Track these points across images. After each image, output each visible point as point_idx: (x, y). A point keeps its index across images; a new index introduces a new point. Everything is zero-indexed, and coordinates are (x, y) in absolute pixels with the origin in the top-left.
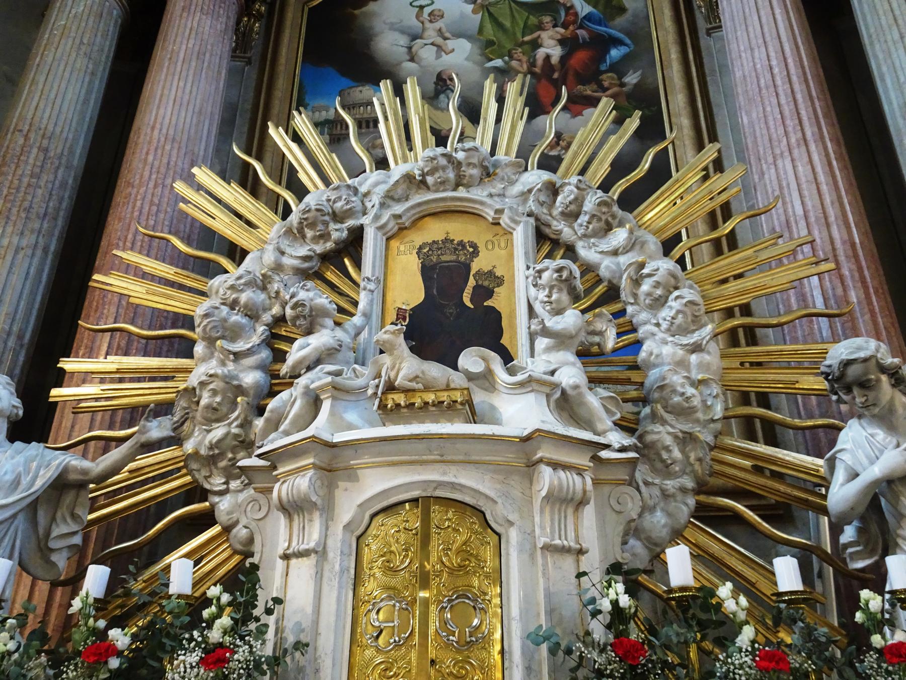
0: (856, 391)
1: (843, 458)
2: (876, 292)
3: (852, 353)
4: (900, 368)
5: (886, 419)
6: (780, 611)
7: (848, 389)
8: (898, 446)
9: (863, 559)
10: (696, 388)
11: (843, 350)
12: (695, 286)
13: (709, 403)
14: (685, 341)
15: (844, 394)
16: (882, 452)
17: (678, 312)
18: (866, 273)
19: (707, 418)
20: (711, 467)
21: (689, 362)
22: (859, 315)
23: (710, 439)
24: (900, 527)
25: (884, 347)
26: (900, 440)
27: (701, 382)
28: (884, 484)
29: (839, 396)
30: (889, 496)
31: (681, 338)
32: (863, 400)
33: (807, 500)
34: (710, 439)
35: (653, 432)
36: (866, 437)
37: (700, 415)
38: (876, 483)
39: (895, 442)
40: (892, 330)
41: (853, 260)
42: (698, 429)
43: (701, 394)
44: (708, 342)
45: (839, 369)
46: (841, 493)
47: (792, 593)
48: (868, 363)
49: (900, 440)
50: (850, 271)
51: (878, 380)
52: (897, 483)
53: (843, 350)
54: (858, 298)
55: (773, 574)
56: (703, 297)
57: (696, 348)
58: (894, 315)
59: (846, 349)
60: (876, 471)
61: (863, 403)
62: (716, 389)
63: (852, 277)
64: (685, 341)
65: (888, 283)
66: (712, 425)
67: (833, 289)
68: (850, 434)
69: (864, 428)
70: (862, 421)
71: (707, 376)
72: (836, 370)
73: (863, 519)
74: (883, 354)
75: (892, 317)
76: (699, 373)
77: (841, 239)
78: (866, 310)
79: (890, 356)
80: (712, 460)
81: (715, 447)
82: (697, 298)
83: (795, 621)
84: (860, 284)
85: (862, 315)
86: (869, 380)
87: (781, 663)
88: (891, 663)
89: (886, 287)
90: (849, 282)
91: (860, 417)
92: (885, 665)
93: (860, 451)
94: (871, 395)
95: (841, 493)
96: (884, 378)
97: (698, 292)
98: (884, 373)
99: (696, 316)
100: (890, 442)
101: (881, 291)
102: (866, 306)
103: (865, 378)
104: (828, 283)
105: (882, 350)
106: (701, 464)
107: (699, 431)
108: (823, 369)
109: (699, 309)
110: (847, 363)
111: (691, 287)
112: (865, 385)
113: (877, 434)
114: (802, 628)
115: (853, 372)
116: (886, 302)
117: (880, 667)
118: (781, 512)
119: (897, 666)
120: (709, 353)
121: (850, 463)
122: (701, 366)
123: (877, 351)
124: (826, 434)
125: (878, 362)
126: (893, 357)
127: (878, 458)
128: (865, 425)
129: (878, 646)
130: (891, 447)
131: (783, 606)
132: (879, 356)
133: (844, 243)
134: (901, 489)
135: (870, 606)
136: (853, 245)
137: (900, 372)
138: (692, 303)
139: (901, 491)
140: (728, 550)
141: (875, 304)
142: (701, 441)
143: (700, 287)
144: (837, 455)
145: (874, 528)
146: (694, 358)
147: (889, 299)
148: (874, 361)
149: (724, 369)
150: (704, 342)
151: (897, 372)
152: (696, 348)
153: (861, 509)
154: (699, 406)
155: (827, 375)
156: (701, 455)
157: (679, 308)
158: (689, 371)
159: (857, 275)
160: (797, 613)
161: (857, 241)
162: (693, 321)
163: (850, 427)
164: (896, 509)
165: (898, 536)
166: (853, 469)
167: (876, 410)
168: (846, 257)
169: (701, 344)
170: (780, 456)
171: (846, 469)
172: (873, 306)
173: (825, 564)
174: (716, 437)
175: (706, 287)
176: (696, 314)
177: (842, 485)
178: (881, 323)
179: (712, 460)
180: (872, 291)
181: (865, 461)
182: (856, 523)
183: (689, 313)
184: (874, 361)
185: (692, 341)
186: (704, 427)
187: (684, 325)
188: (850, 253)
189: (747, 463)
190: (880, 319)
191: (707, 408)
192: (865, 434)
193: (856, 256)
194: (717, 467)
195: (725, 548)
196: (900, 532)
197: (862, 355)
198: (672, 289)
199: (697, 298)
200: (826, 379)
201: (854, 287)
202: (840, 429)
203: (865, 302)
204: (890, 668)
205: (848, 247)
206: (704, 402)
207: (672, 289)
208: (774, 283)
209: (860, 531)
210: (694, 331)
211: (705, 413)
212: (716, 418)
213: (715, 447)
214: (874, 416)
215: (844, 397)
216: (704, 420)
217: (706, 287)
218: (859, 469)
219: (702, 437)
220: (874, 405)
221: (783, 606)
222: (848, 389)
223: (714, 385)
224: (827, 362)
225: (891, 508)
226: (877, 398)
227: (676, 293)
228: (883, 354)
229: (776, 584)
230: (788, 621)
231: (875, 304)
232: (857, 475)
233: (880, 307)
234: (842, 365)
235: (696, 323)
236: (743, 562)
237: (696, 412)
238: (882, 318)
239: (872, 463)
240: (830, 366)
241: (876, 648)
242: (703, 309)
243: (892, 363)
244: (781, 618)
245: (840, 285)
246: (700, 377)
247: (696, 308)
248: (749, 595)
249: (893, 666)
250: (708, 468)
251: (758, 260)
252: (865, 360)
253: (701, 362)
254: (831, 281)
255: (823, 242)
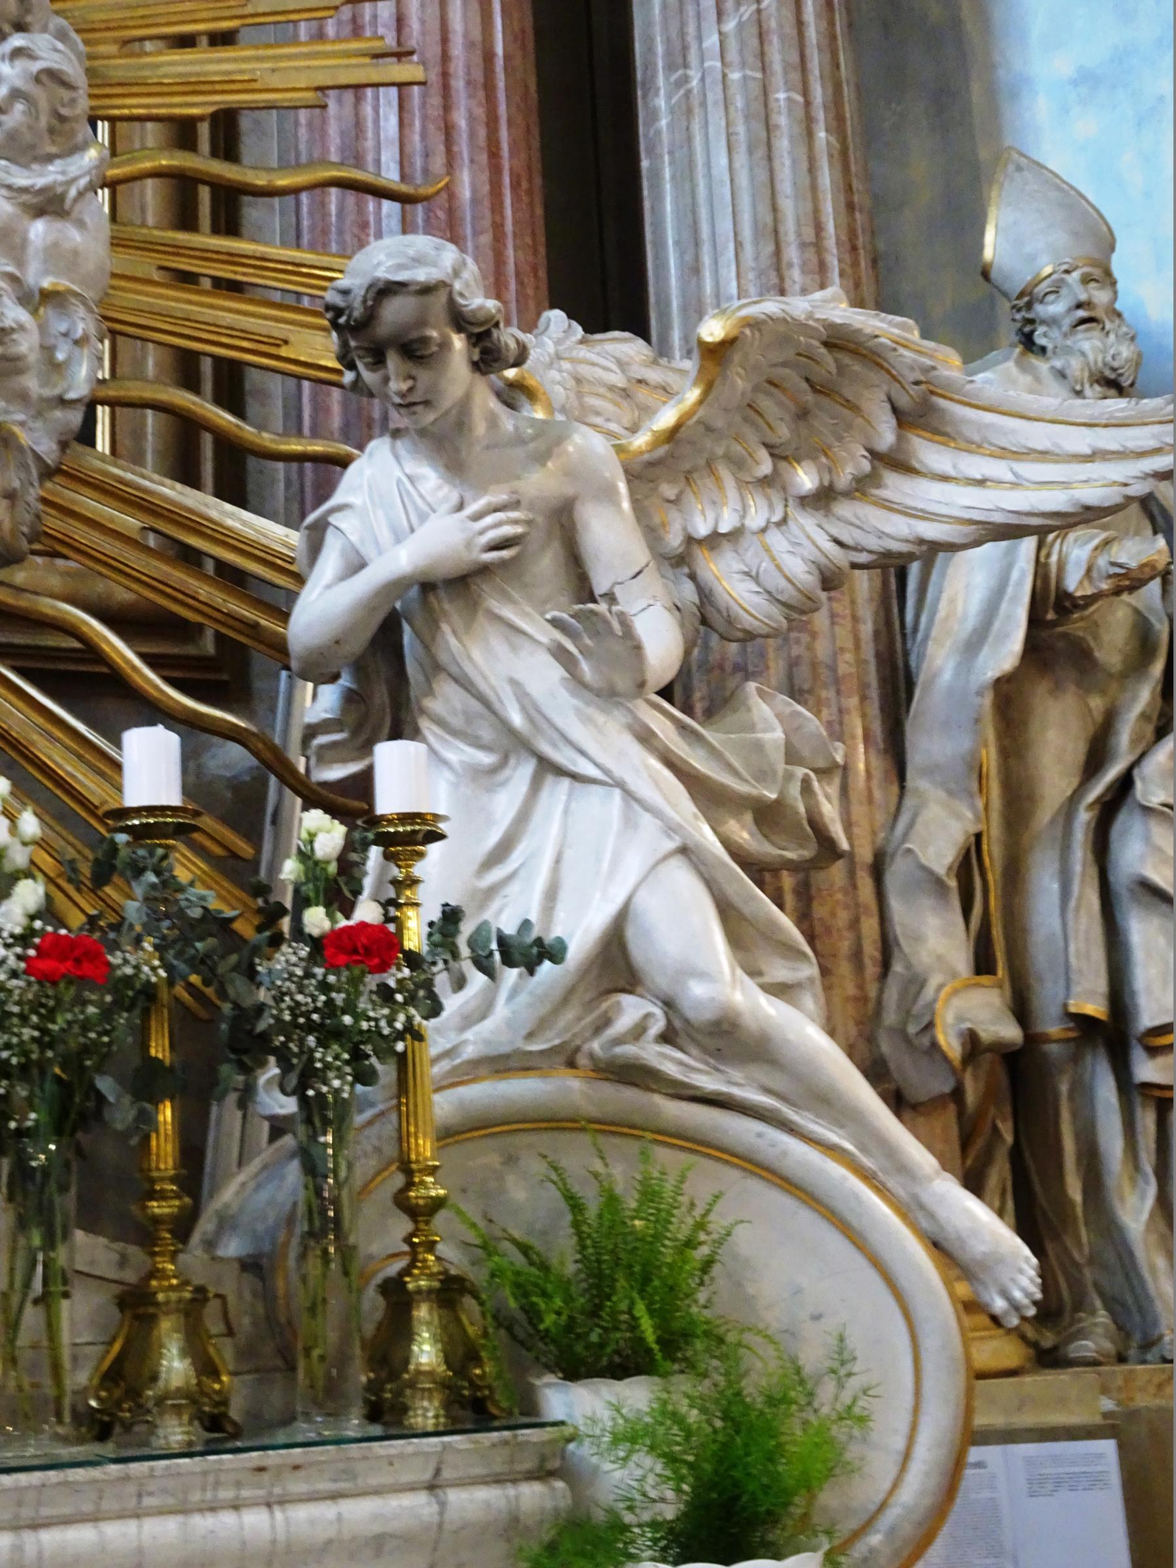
0: (393, 361)
1: (342, 526)
2: (515, 186)
3: (401, 267)
4: (497, 325)
5: (447, 444)
6: (114, 848)
7: (378, 359)
8: (460, 507)
9: (344, 761)
10: (34, 312)
11: (382, 257)
12: (74, 35)
13: (60, 356)
14: (22, 178)
15: (366, 365)
16: (423, 518)
17: (16, 94)
18: (504, 134)
19: (48, 392)
20: (38, 517)
21: (25, 242)
22: (469, 231)
23: (47, 448)
24: (430, 692)
25: (471, 269)
26: (468, 495)
27: (48, 296)
28: (414, 592)
29: (358, 375)
30: (419, 621)
31: (14, 168)
32: (404, 386)
33: (255, 626)
34: (47, 448)
35: (1028, 1295)
36: (399, 482)
37: (32, 383)
38: (397, 586)
39: (454, 498)
40: (529, 281)
41: (481, 94)
42: (21, 417)
43: (43, 328)
44: (81, 194)
45: (364, 301)
46: (323, 606)
47: (151, 810)
48: (429, 299)
49: (468, 495)
50: (471, 119)
51: (445, 345)
52: (442, 593)
53: (382, 257)
54: (474, 190)
55: (118, 767)
56: (90, 72)
57: (49, 204)
58: (542, 250)
59: (389, 255)
60: (399, 559)
61: (403, 395)
62: (83, 323)
63: (472, 135)
64: (22, 178)
65: (545, 176)
66: (58, 414)
67: (427, 155)
68: (368, 472)
69: (397, 457)
70: (399, 443)
71: (64, 283)
72: (357, 304)
73: (360, 667)
74: (467, 285)
75: (535, 252)
76: (46, 272)
77: (466, 35)
78: (487, 223)
79: (481, 292)
80: (44, 501)
81: (58, 471)
82: (73, 70)
83: (139, 872)
84: (483, 158)
85: (476, 233)
86: (425, 341)
87: (85, 965)
88: (332, 967)
89: (538, 181)
90: (463, 146)
91: (396, 434)
92: (319, 971)
93: (380, 513)
94: (424, 376)
95: (323, 606)
96: (458, 342)
97: (79, 55)
98: (459, 329)
99: (62, 119)
100: (446, 499)
101: (525, 185)
102: (488, 214)
103: (414, 335)
104: (417, 138)
105: (466, 275)
106: (13, 506)
107: (22, 424)
108: (331, 297)
109: (73, 101)
110: (386, 290)
111: (62, 36)
112: (415, 350)
113: (424, 477)
114: (153, 886)
115: (395, 312)
116: (532, 216)
117: (308, 975)
118: (225, 677)
119: (345, 974)
120: (81, 224)
121: (354, 538)
122: (54, 254)
123: (456, 273)
124: (315, 472)
125: (451, 302)
126: (487, 297)
127: (412, 530)
128: (402, 452)
129: (316, 932)
130: (445, 507)
131: (122, 838)
132: (457, 286)
133: (470, 45)
134: (447, 606)
135: (317, 846)
136: (488, 57)
137: (495, 333)
138: (53, 76)
139: (443, 611)
140: (49, 727)
141: (508, 212)
142: (20, 449)
143: (87, 42)
144: (331, 519)
145: (381, 695)
146: (38, 230)
147: (539, 211)
148: (442, 297)
149: (114, 275)
150: (73, 192)
151: (488, 333)
152: (49, 204)
153: (358, 644)
154: (33, 357)
155: (338, 311)
156: (16, 484)
157: (19, 83)
158: (20, 263)
159: (482, 133)
160: (152, 854)
161: (499, 49)
162: (51, 131)
163: (371, 454)
164: (427, 647)
165: (423, 711)
166: (357, 552)
167: (428, 417)
168: (469, 83)
169: (61, 198)
170: (214, 514)
171: (343, 553)
172: (503, 217)
173: (288, 792)
174: (64, 445)
175: (102, 49)
176: (64, 111)
177: (328, 587)
178: (511, 261)
179: (44, 501)
180: (507, 180)
181: (385, 535)
182: (345, 681)
183: (43, 105)
184: (442, 297)
185: (40, 182)
186: (39, 414)
187: (28, 137)
188: (478, 75)
189: (130, 522)
190: (510, 252)
191: (55, 368)
192: (398, 473)
193: (489, 87)
194: (54, 523)
195: (40, 721)
196: (429, 704)
197: (421, 275)
198: (7, 28)
199: (73, 70)
200: (335, 325)
201: (472, 161)
202: (343, 462)
203: (487, 203)
204: (332, 979)
205: (478, 59)
206: (48, 350)
207: (7, 28)
208: (275, 81)
209: (350, 698)
210: (50, 158)
211: (45, 384)
212: (72, 395)
213: (58, 471)
214: (423, 433)
215: (368, 376)
216: (42, 399)
217: (102, 49)
218: (368, 551)
219: (24, 437)
220: (427, 403)
221: (122, 838)
222: (378, 359)
223: (81, 311)
224: (344, 282)
225: (420, 648)
226: (434, 388)
227: (17, 40)
228: (467, 285)
229: (119, 789)
230: (129, 873)
231: (508, 212)
232: (362, 565)
233: (515, 222)
234: (371, 295)
235: (61, 136)
236: (80, 757)
237: (20, 372)
238: (516, 248)
239: (398, 540)
240: (345, 292)
241: (310, 936)
242: (84, 104)
243: (481, 308)
244: (113, 868)
245: (442, 148)
246: (47, 283)
247: (65, 94)
248: (51, 812)
249: (338, 974)
250: (28, 518)
251: (249, 9)
252: (426, 290)
253: (56, 245)
254: (424, 135)
255: (424, 33)
